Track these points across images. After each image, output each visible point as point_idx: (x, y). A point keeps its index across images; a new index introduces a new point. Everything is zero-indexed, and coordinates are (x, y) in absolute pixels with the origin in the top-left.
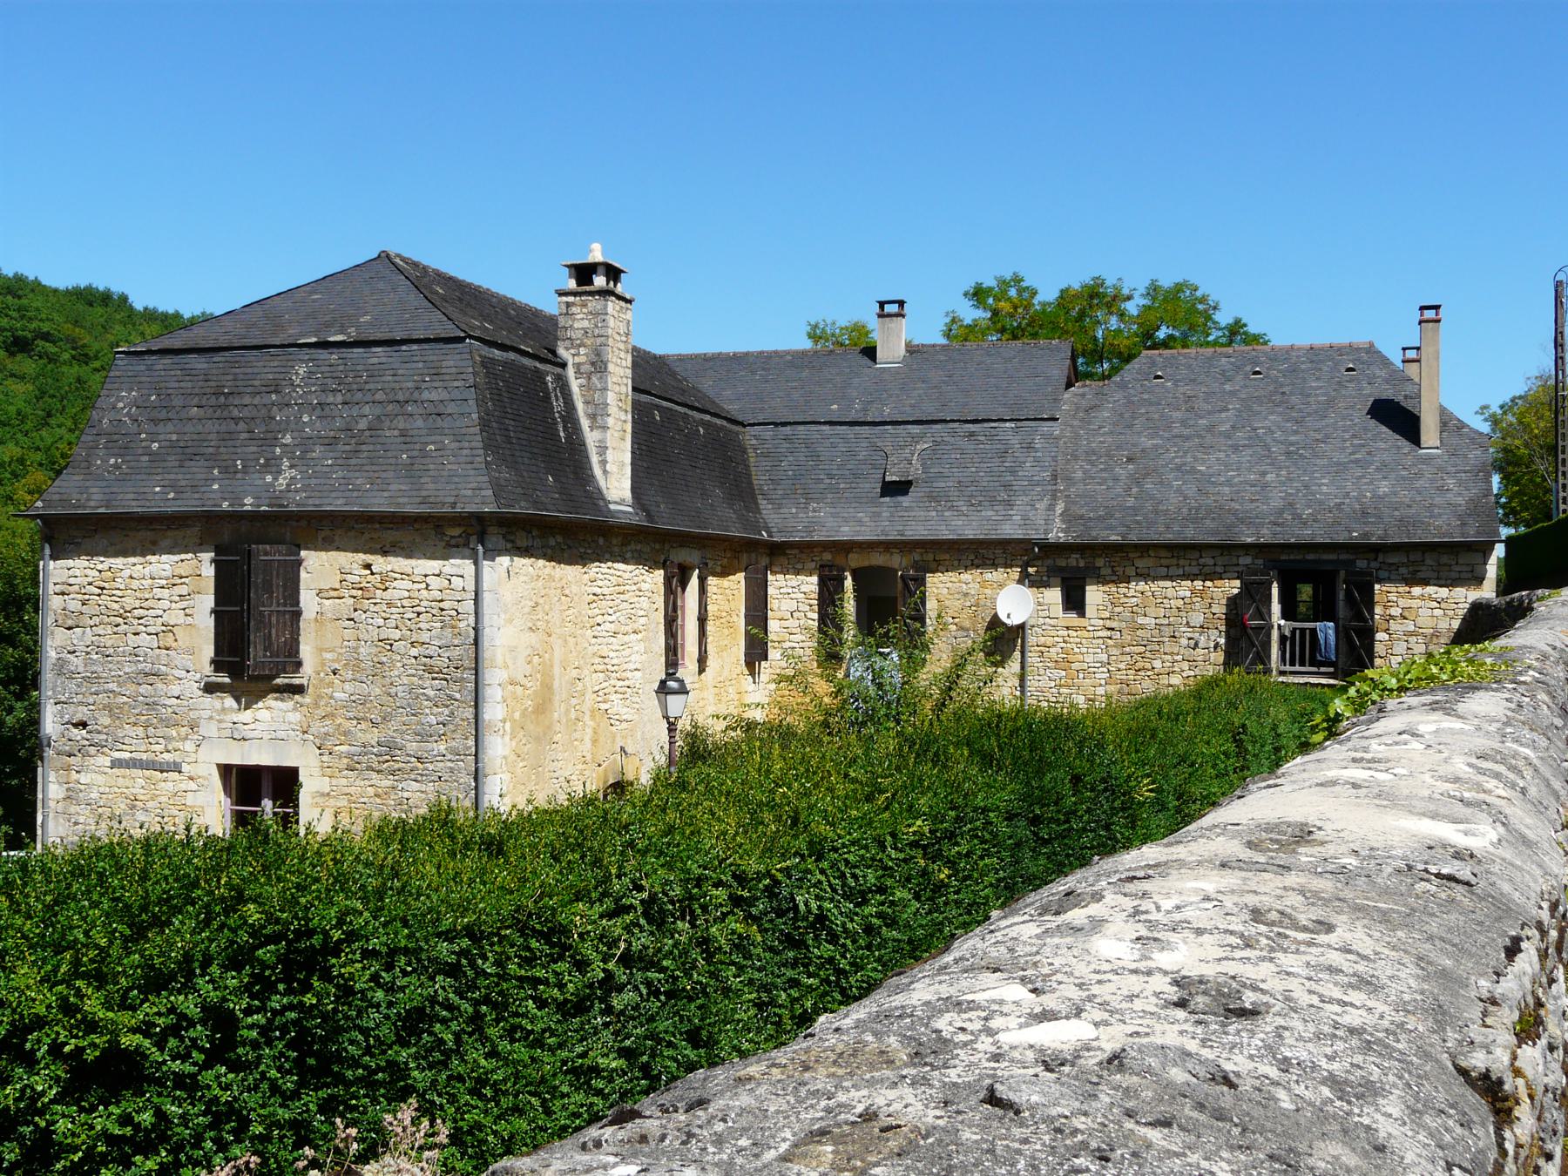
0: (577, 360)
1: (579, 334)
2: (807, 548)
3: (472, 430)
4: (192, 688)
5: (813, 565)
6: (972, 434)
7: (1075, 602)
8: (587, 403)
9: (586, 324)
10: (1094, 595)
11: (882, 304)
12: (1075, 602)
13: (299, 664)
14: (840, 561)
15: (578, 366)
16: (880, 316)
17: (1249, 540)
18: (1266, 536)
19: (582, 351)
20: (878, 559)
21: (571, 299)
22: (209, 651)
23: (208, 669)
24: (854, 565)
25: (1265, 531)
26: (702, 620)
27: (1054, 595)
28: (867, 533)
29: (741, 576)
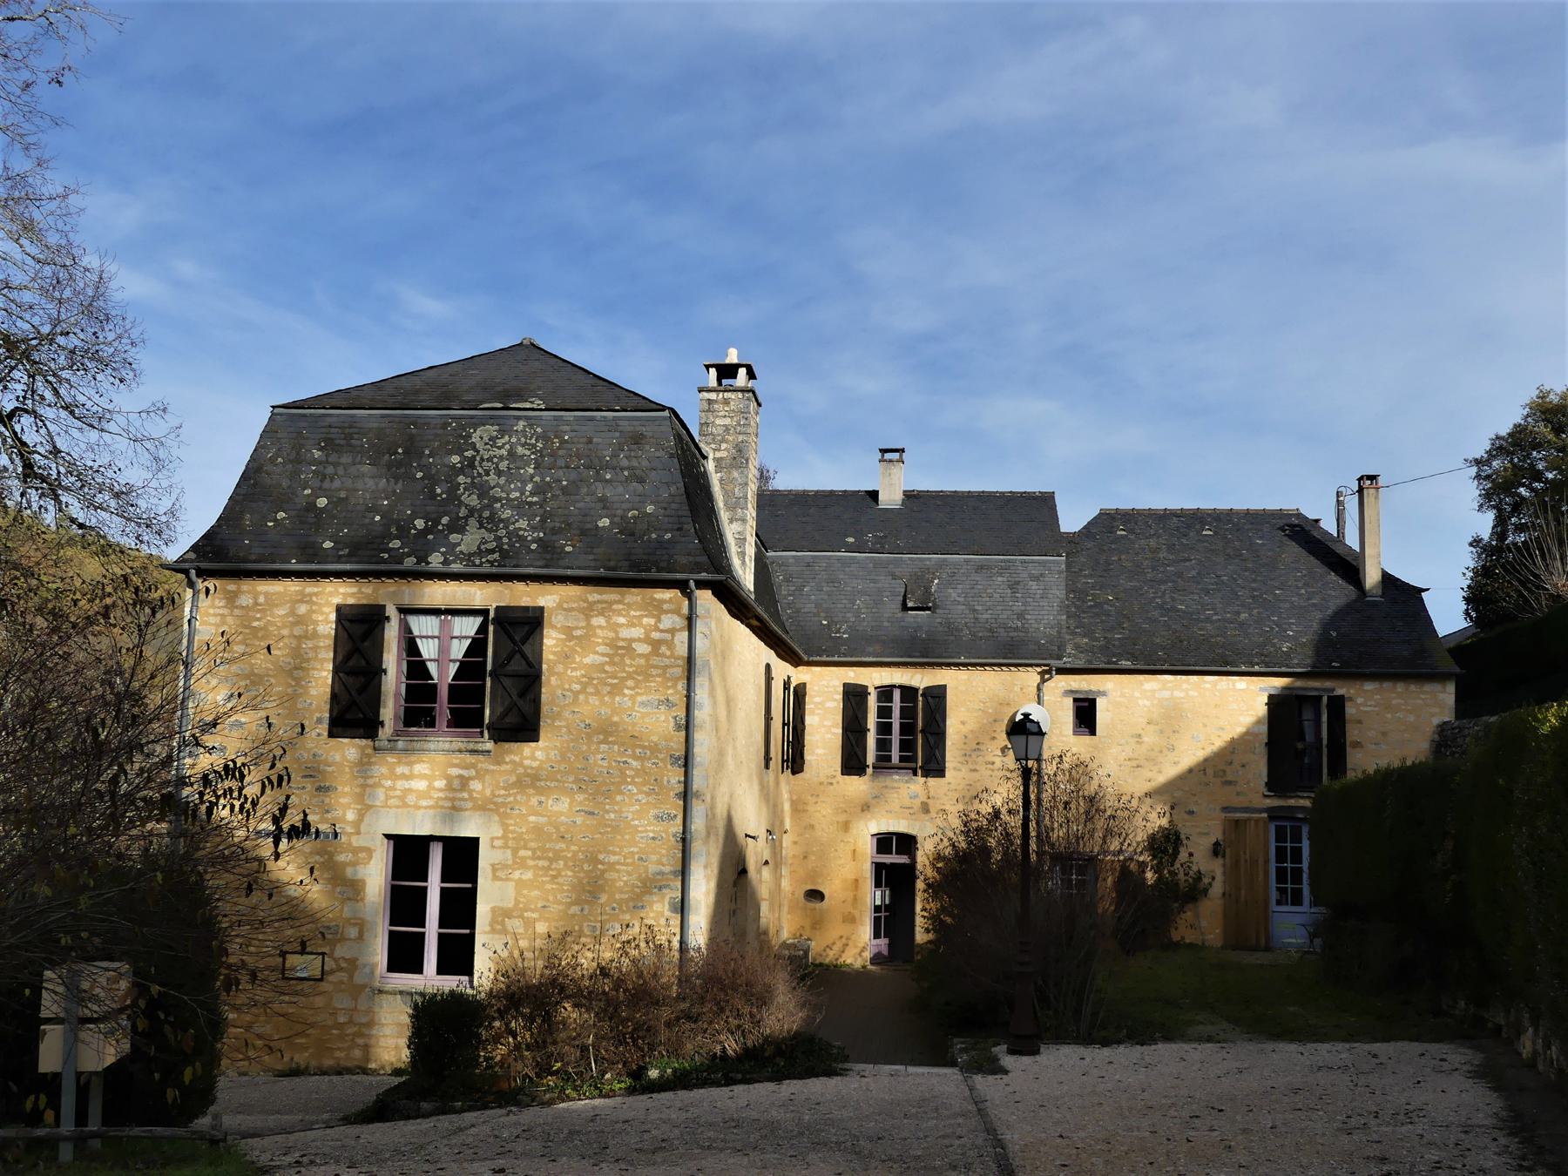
0: (718, 455)
9: (727, 421)
19: (724, 446)
21: (713, 396)
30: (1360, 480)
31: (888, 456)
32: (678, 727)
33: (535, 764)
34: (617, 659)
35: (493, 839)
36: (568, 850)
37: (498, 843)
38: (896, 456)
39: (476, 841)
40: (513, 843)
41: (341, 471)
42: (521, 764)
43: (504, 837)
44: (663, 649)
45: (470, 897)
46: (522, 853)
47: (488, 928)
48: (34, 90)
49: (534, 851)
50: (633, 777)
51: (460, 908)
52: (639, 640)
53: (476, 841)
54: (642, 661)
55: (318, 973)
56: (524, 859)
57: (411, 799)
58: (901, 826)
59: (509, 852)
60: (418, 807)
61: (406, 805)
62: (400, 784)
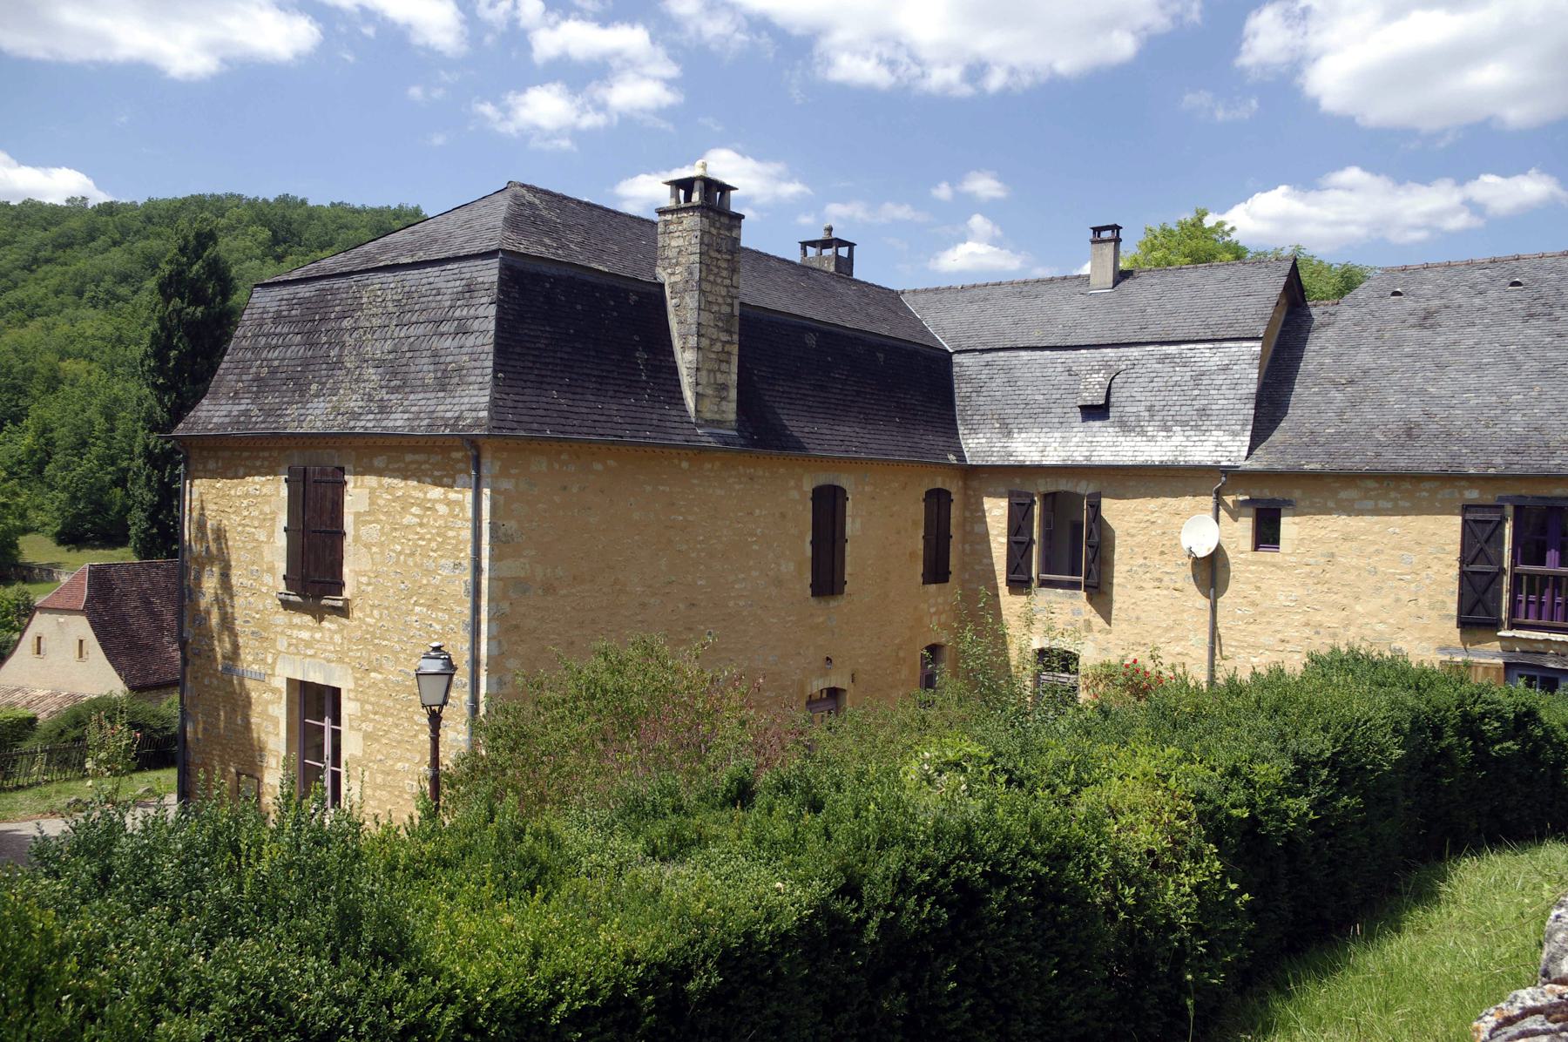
0: (673, 279)
2: (1450, 478)
3: (486, 348)
4: (272, 603)
5: (1002, 490)
6: (1167, 356)
7: (1267, 535)
8: (680, 323)
9: (680, 242)
10: (1290, 527)
11: (1097, 230)
12: (1267, 535)
13: (341, 585)
14: (1029, 488)
15: (673, 285)
16: (1093, 242)
17: (1472, 471)
18: (1498, 464)
19: (678, 269)
20: (1063, 485)
22: (282, 568)
23: (282, 587)
24: (1043, 489)
25: (1498, 460)
26: (477, 569)
27: (1244, 528)
28: (1053, 458)
29: (986, 500)
61: (298, 653)
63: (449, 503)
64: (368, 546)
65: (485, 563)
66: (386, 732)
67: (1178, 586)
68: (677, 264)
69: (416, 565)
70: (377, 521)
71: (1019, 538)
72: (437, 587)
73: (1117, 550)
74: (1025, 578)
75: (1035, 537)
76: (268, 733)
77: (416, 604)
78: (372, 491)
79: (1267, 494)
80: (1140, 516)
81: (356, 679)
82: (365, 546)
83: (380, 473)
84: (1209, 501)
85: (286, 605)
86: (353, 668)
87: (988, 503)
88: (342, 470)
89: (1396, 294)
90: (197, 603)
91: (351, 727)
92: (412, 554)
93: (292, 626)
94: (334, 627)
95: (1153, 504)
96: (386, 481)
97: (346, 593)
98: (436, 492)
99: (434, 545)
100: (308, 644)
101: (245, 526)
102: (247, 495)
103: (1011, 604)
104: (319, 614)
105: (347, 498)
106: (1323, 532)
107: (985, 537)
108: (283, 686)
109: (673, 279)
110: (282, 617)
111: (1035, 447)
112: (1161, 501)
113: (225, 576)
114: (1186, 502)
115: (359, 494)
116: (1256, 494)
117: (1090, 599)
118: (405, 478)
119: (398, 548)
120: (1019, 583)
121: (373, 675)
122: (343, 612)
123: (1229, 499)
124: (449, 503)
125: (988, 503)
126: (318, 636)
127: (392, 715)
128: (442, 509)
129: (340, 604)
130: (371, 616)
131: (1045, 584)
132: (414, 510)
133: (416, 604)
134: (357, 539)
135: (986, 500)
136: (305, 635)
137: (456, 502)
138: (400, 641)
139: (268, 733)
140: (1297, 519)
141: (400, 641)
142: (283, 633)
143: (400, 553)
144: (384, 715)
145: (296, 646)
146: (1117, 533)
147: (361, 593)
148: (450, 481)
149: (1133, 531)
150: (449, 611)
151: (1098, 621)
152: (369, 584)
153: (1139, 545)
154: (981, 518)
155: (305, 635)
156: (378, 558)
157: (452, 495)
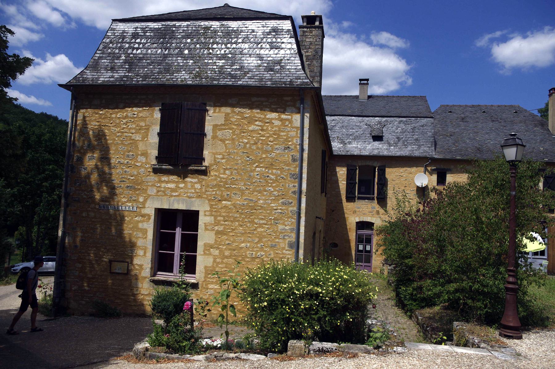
0: (307, 54)
1: (308, 44)
9: (311, 40)
15: (307, 56)
19: (310, 50)
21: (306, 30)
23: (154, 162)
24: (360, 164)
26: (302, 150)
29: (337, 168)
30: (550, 91)
31: (362, 82)
32: (294, 160)
33: (225, 176)
34: (265, 128)
35: (205, 211)
36: (240, 217)
37: (207, 213)
38: (366, 82)
39: (198, 211)
40: (212, 212)
41: (141, 46)
42: (219, 177)
43: (210, 211)
44: (287, 123)
45: (195, 238)
46: (219, 218)
47: (202, 253)
48: (435, 177)
49: (224, 217)
50: (271, 183)
51: (190, 243)
52: (276, 119)
53: (198, 211)
54: (277, 129)
55: (126, 272)
56: (219, 221)
57: (168, 192)
58: (368, 219)
59: (213, 217)
60: (172, 196)
61: (166, 195)
62: (163, 185)
63: (282, 120)
64: (223, 141)
65: (306, 147)
66: (233, 230)
67: (411, 198)
68: (309, 48)
69: (258, 148)
70: (230, 129)
71: (351, 182)
72: (272, 158)
73: (389, 186)
74: (354, 196)
75: (357, 181)
76: (137, 238)
77: (257, 167)
78: (227, 115)
79: (442, 167)
80: (397, 174)
81: (211, 206)
82: (221, 140)
83: (233, 106)
84: (422, 169)
85: (156, 171)
86: (209, 200)
87: (338, 169)
88: (205, 105)
89: (450, 112)
90: (79, 172)
91: (206, 229)
92: (256, 143)
93: (160, 181)
94: (194, 180)
95: (402, 170)
96: (237, 110)
97: (206, 163)
98: (274, 115)
99: (271, 139)
100: (173, 190)
101: (122, 132)
102: (126, 117)
103: (348, 206)
104: (183, 174)
105: (207, 118)
106: (461, 179)
107: (337, 182)
108: (152, 213)
109: (307, 54)
110: (153, 178)
111: (357, 147)
112: (405, 169)
113: (105, 158)
114: (414, 169)
115: (214, 117)
116: (438, 167)
117: (378, 203)
118: (251, 108)
119: (246, 141)
120: (351, 198)
121: (224, 202)
122: (204, 173)
123: (429, 168)
124: (282, 120)
125: (338, 169)
126: (182, 185)
127: (238, 221)
128: (277, 123)
129: (204, 168)
130: (224, 174)
131: (359, 198)
132: (257, 123)
133: (257, 167)
134: (214, 137)
135: (337, 168)
136: (172, 186)
137: (286, 120)
138: (245, 185)
139: (137, 238)
140: (452, 175)
141: (245, 185)
142: (153, 185)
143: (247, 143)
144: (232, 221)
145: (164, 192)
146: (389, 180)
147: (216, 163)
148: (282, 110)
149: (394, 179)
150: (282, 169)
151: (382, 211)
152: (222, 159)
153: (397, 184)
154: (335, 174)
155: (172, 186)
156: (229, 146)
157: (283, 116)
